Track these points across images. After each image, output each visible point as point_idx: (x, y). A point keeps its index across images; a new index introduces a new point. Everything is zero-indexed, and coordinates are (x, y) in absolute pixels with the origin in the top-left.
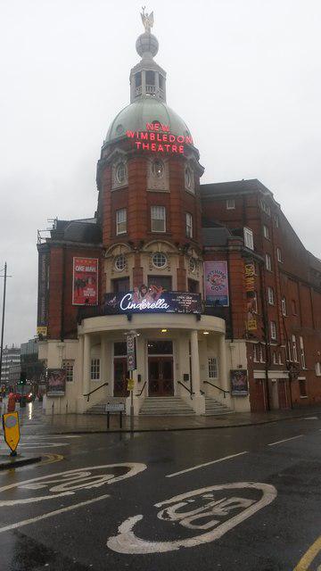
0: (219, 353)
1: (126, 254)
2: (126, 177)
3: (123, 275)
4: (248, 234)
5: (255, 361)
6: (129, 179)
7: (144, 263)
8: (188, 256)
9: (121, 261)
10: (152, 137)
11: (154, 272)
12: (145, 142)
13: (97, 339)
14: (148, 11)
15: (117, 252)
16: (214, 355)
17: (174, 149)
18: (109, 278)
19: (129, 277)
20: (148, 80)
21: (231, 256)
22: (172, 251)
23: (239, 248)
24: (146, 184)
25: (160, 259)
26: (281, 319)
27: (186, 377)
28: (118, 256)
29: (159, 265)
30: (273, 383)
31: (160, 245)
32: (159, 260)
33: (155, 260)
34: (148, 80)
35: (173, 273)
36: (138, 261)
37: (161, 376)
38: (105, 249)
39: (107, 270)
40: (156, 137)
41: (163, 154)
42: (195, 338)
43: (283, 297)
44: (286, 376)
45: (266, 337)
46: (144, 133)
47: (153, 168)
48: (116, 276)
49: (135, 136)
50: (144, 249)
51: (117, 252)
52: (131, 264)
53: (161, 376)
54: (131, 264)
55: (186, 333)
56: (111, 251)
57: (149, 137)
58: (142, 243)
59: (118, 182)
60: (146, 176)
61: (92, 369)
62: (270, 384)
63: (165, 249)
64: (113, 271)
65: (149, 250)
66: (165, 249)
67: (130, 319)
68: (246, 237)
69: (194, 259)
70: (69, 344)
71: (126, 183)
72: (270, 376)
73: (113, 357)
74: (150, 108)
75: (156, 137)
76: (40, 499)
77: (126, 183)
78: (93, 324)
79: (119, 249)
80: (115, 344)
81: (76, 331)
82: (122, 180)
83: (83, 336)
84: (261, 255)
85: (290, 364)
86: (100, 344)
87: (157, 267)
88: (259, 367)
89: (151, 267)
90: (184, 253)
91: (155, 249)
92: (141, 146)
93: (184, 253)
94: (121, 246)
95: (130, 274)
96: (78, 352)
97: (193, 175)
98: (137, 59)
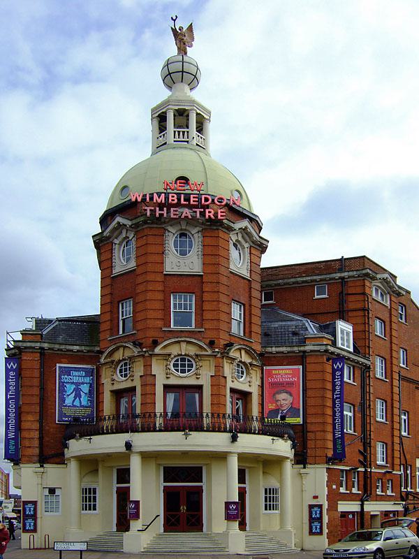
0: (281, 481)
1: (130, 358)
2: (133, 256)
3: (128, 385)
4: (344, 328)
5: (342, 490)
7: (157, 368)
8: (229, 358)
10: (173, 199)
12: (161, 206)
13: (90, 464)
14: (182, 24)
16: (273, 483)
17: (209, 213)
18: (107, 388)
19: (133, 389)
20: (178, 121)
21: (309, 360)
22: (206, 353)
23: (323, 348)
25: (184, 363)
26: (397, 440)
28: (120, 361)
30: (373, 517)
31: (184, 345)
32: (183, 365)
34: (178, 121)
35: (205, 380)
36: (148, 366)
37: (183, 508)
38: (101, 352)
39: (105, 380)
40: (179, 199)
41: (192, 221)
43: (406, 412)
46: (159, 194)
48: (117, 387)
49: (144, 199)
50: (157, 350)
52: (139, 370)
53: (183, 508)
54: (139, 370)
55: (222, 457)
56: (111, 354)
57: (167, 198)
58: (155, 343)
59: (123, 262)
62: (367, 518)
63: (192, 350)
66: (192, 350)
68: (339, 335)
69: (244, 363)
70: (52, 470)
72: (366, 508)
73: (163, 484)
74: (181, 161)
75: (179, 199)
77: (132, 264)
78: (77, 447)
79: (121, 350)
81: (63, 454)
82: (128, 260)
83: (69, 459)
84: (364, 357)
85: (408, 493)
86: (97, 471)
88: (349, 497)
90: (225, 355)
91: (174, 350)
92: (153, 212)
93: (225, 355)
94: (125, 347)
95: (137, 383)
96: (67, 478)
97: (247, 251)
98: (163, 94)
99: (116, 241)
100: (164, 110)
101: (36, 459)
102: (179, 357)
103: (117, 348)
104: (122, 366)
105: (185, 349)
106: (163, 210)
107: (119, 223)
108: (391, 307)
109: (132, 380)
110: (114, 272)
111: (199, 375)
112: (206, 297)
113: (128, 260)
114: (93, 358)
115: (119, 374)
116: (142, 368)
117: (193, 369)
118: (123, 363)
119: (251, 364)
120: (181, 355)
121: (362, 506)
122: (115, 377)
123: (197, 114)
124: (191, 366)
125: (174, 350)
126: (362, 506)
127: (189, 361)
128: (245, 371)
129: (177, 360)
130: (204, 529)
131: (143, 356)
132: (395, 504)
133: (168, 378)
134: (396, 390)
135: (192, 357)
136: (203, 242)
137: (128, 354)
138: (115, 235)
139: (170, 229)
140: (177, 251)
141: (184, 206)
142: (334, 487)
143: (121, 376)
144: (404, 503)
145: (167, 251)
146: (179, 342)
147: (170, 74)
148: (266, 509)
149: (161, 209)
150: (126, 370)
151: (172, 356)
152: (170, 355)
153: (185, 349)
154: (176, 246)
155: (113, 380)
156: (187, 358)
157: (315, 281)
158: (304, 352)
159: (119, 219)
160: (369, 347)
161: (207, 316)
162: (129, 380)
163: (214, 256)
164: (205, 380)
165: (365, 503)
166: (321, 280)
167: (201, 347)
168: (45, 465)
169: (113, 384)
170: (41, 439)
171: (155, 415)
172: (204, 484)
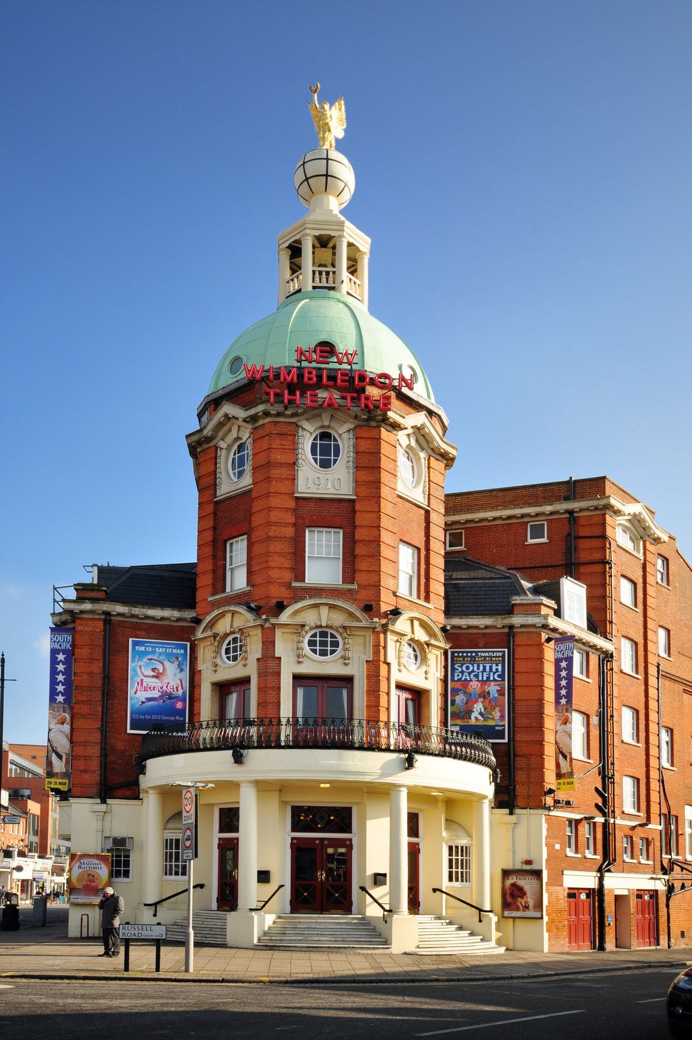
6: (255, 469)
7: (283, 648)
9: (235, 652)
11: (307, 668)
15: (223, 626)
21: (519, 640)
24: (293, 479)
27: (379, 879)
29: (323, 653)
31: (324, 611)
32: (323, 644)
33: (312, 643)
36: (269, 644)
38: (197, 621)
39: (203, 665)
42: (285, 732)
44: (660, 886)
45: (606, 805)
47: (314, 447)
51: (223, 626)
52: (255, 650)
55: (381, 792)
56: (212, 624)
58: (280, 607)
60: (294, 463)
61: (168, 857)
64: (216, 666)
65: (298, 620)
66: (338, 619)
67: (238, 759)
69: (418, 642)
71: (247, 480)
76: (384, 1017)
77: (247, 480)
78: (162, 770)
79: (228, 617)
80: (221, 810)
81: (136, 783)
85: (672, 863)
87: (317, 657)
89: (300, 658)
91: (310, 618)
94: (234, 613)
95: (252, 670)
99: (223, 445)
100: (297, 238)
101: (95, 790)
102: (318, 631)
103: (222, 615)
104: (229, 644)
105: (325, 616)
106: (295, 395)
107: (226, 415)
108: (645, 560)
109: (245, 665)
110: (218, 494)
111: (349, 659)
112: (360, 534)
113: (240, 474)
114: (182, 634)
115: (224, 656)
116: (260, 645)
117: (339, 649)
118: (230, 638)
119: (428, 645)
120: (321, 626)
121: (601, 879)
122: (218, 661)
123: (350, 245)
124: (335, 644)
125: (310, 618)
126: (601, 879)
127: (333, 636)
128: (419, 656)
129: (314, 635)
130: (354, 908)
131: (262, 626)
132: (652, 878)
133: (299, 662)
134: (652, 692)
135: (337, 631)
136: (356, 446)
137: (239, 623)
138: (221, 434)
139: (306, 425)
140: (315, 460)
141: (326, 387)
142: (558, 847)
143: (228, 658)
144: (667, 877)
145: (300, 461)
146: (316, 606)
147: (307, 179)
148: (451, 879)
149: (292, 392)
150: (235, 650)
151: (307, 628)
152: (303, 626)
153: (325, 616)
154: (314, 452)
155: (216, 667)
156: (330, 631)
157: (529, 515)
158: (511, 627)
159: (228, 409)
160: (611, 622)
161: (362, 565)
162: (240, 666)
163: (369, 467)
164: (357, 669)
165: (606, 874)
166: (537, 515)
167: (351, 615)
168: (109, 801)
169: (215, 671)
170: (104, 755)
171: (279, 721)
172: (354, 836)
